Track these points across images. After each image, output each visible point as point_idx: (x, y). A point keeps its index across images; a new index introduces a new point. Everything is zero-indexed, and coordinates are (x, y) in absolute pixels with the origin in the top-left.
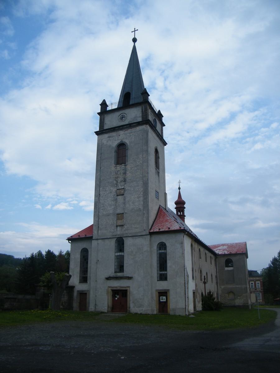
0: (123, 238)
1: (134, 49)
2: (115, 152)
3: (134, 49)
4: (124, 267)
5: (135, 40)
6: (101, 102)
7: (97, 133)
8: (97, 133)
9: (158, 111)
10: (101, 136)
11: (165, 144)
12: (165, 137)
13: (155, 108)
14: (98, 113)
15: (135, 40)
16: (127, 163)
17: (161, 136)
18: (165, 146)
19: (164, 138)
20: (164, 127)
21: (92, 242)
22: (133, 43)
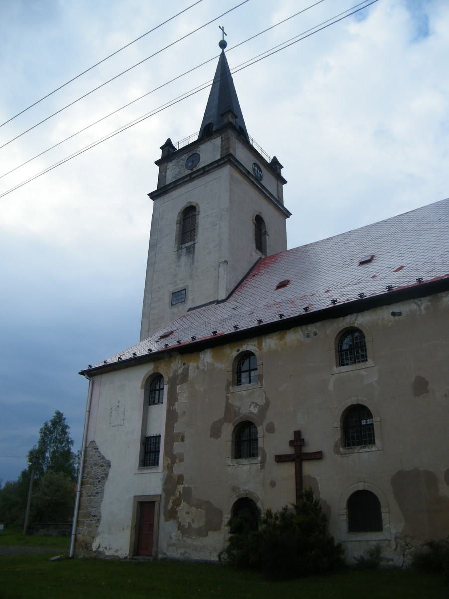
0: (248, 359)
1: (223, 58)
2: (177, 224)
3: (223, 58)
4: (282, 455)
5: (223, 45)
6: (163, 143)
7: (152, 196)
8: (152, 196)
9: (272, 158)
10: (159, 200)
11: (287, 214)
12: (287, 204)
13: (265, 153)
14: (157, 163)
15: (223, 45)
16: (196, 240)
17: (278, 201)
18: (287, 219)
19: (285, 206)
20: (284, 186)
21: (199, 356)
22: (220, 51)
